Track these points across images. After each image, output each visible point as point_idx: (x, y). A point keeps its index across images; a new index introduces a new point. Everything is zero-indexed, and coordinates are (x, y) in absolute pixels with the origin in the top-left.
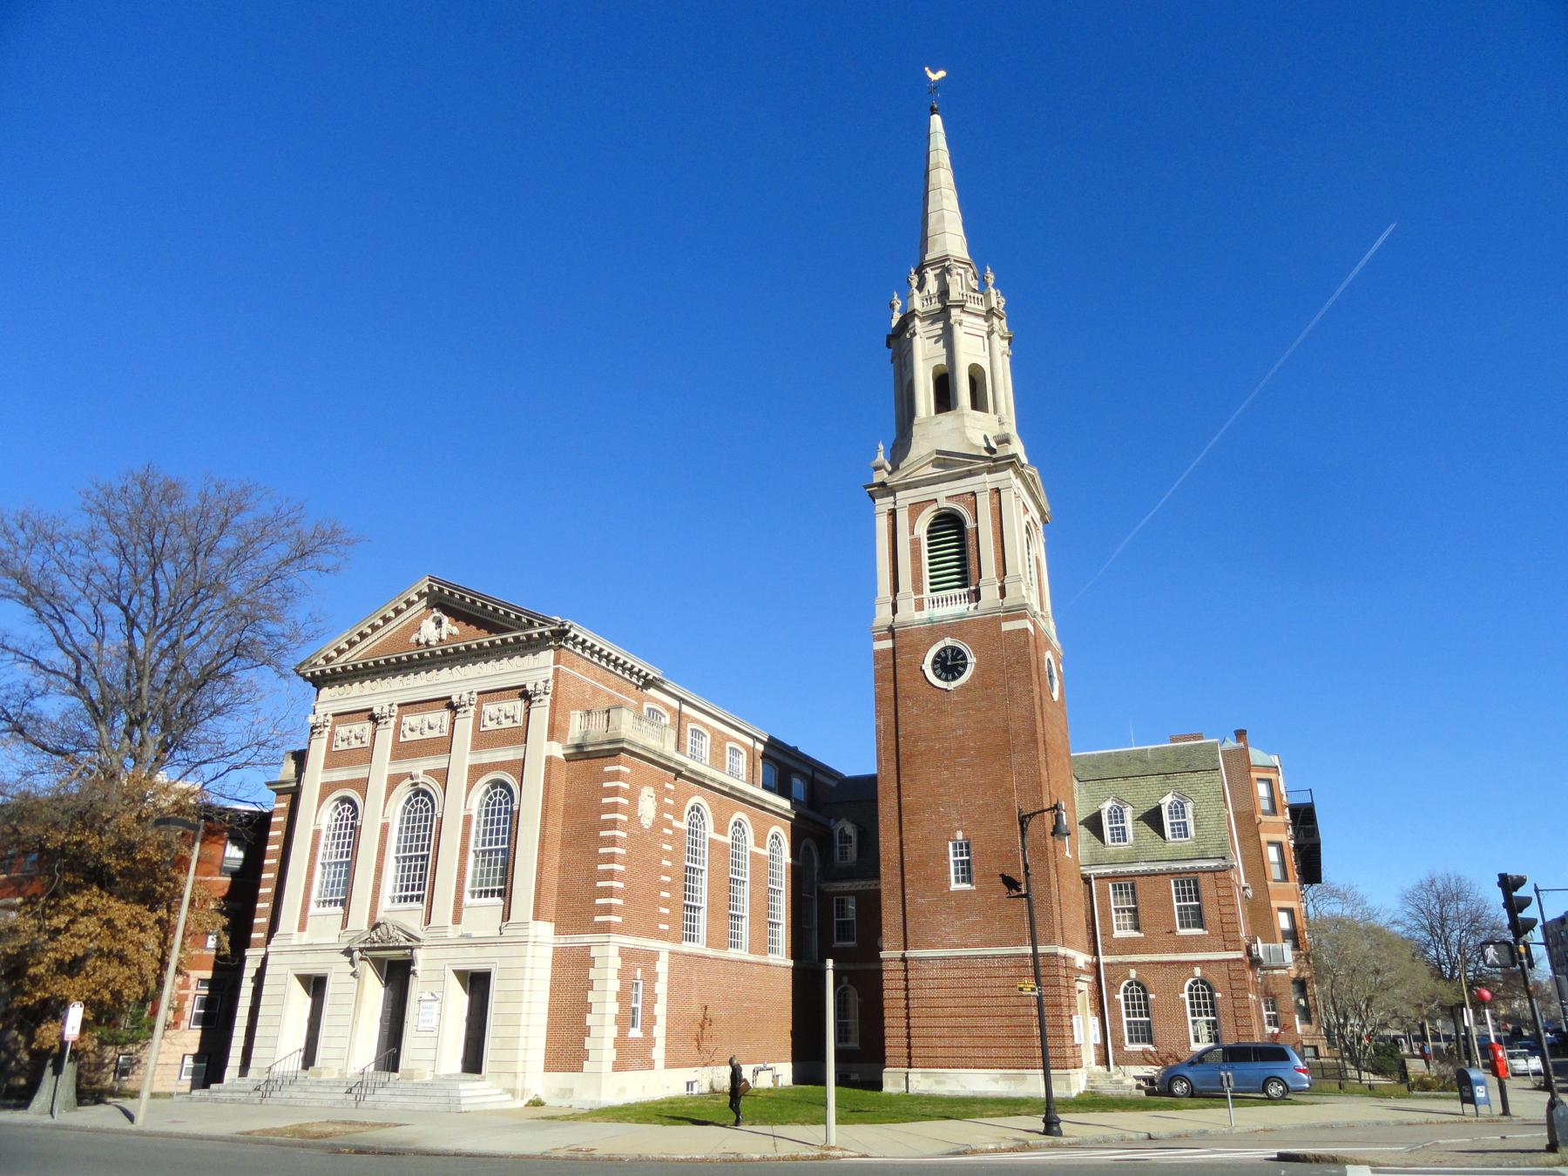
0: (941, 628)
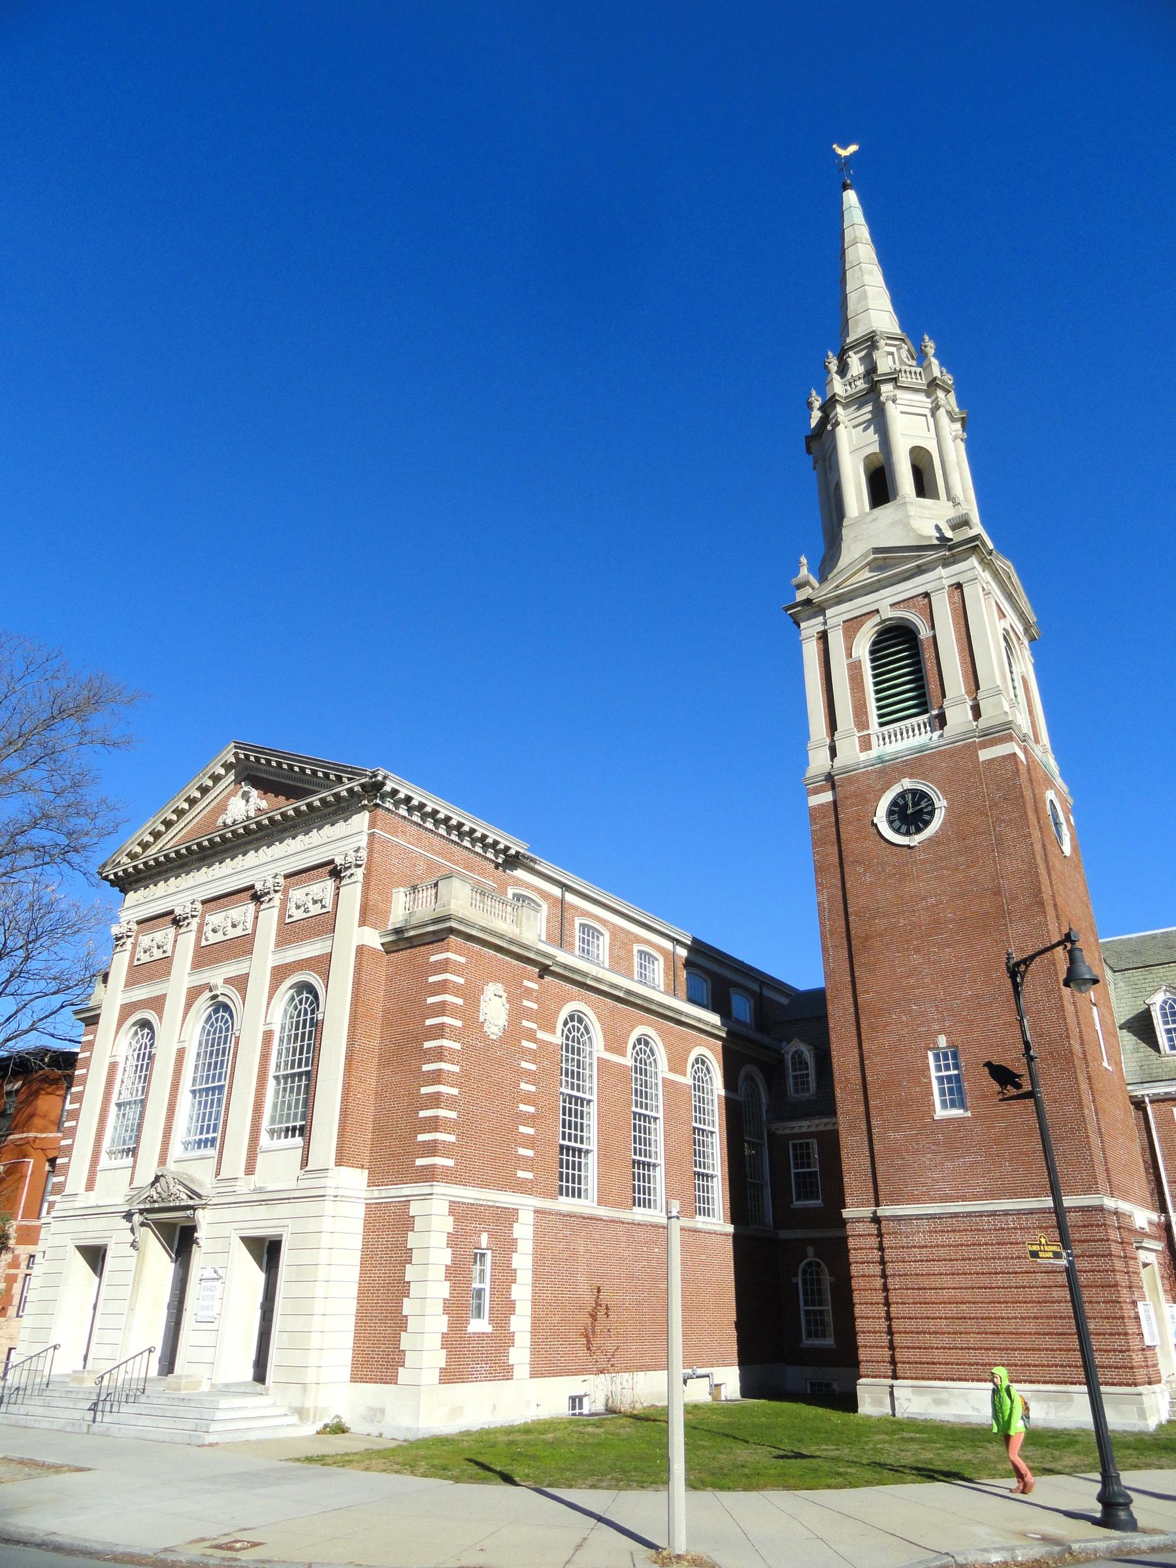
0: (895, 768)
